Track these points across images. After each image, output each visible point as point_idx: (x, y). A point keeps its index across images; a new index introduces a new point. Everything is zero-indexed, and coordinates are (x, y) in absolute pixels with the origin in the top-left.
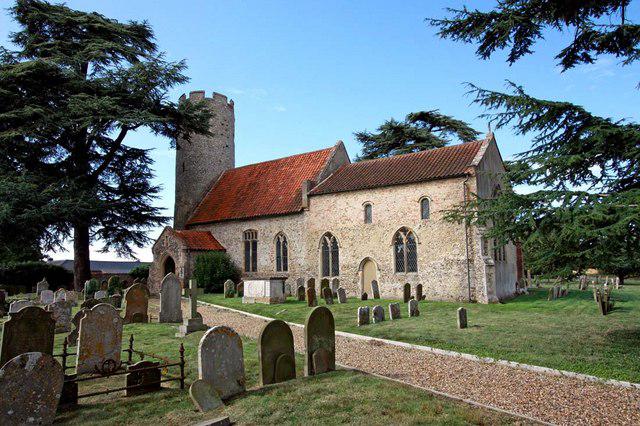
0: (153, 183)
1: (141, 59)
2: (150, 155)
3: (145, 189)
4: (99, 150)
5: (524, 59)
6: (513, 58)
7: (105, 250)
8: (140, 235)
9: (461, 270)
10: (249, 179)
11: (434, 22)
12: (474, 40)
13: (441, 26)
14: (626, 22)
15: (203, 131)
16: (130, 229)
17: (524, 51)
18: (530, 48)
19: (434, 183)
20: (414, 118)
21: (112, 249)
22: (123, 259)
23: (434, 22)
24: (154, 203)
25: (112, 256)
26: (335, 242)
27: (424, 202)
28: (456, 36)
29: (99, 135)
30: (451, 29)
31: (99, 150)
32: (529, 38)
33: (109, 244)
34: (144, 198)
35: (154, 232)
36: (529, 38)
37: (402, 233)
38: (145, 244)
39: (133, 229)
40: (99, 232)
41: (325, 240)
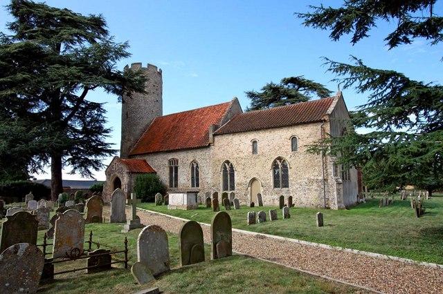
0: (106, 126)
1: (98, 40)
2: (104, 107)
3: (100, 130)
4: (68, 103)
5: (362, 41)
6: (355, 40)
7: (73, 172)
8: (97, 162)
9: (319, 186)
10: (172, 124)
11: (300, 15)
12: (328, 28)
13: (305, 18)
14: (433, 15)
15: (141, 91)
16: (90, 158)
17: (363, 35)
18: (367, 33)
19: (300, 126)
20: (287, 81)
21: (77, 172)
22: (85, 179)
23: (300, 15)
24: (107, 140)
25: (77, 177)
26: (232, 167)
27: (294, 139)
28: (315, 25)
29: (68, 93)
30: (312, 20)
31: (68, 103)
32: (366, 26)
33: (75, 168)
34: (100, 136)
35: (107, 160)
36: (366, 26)
37: (278, 161)
38: (100, 169)
39: (92, 158)
40: (69, 160)
41: (225, 166)
